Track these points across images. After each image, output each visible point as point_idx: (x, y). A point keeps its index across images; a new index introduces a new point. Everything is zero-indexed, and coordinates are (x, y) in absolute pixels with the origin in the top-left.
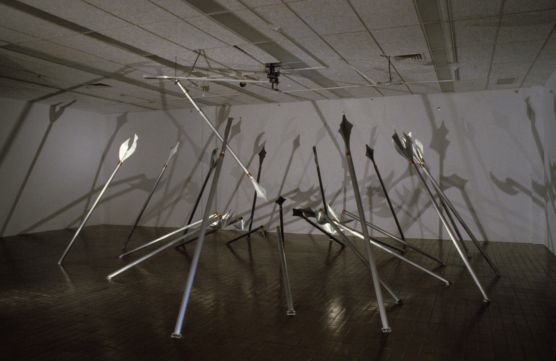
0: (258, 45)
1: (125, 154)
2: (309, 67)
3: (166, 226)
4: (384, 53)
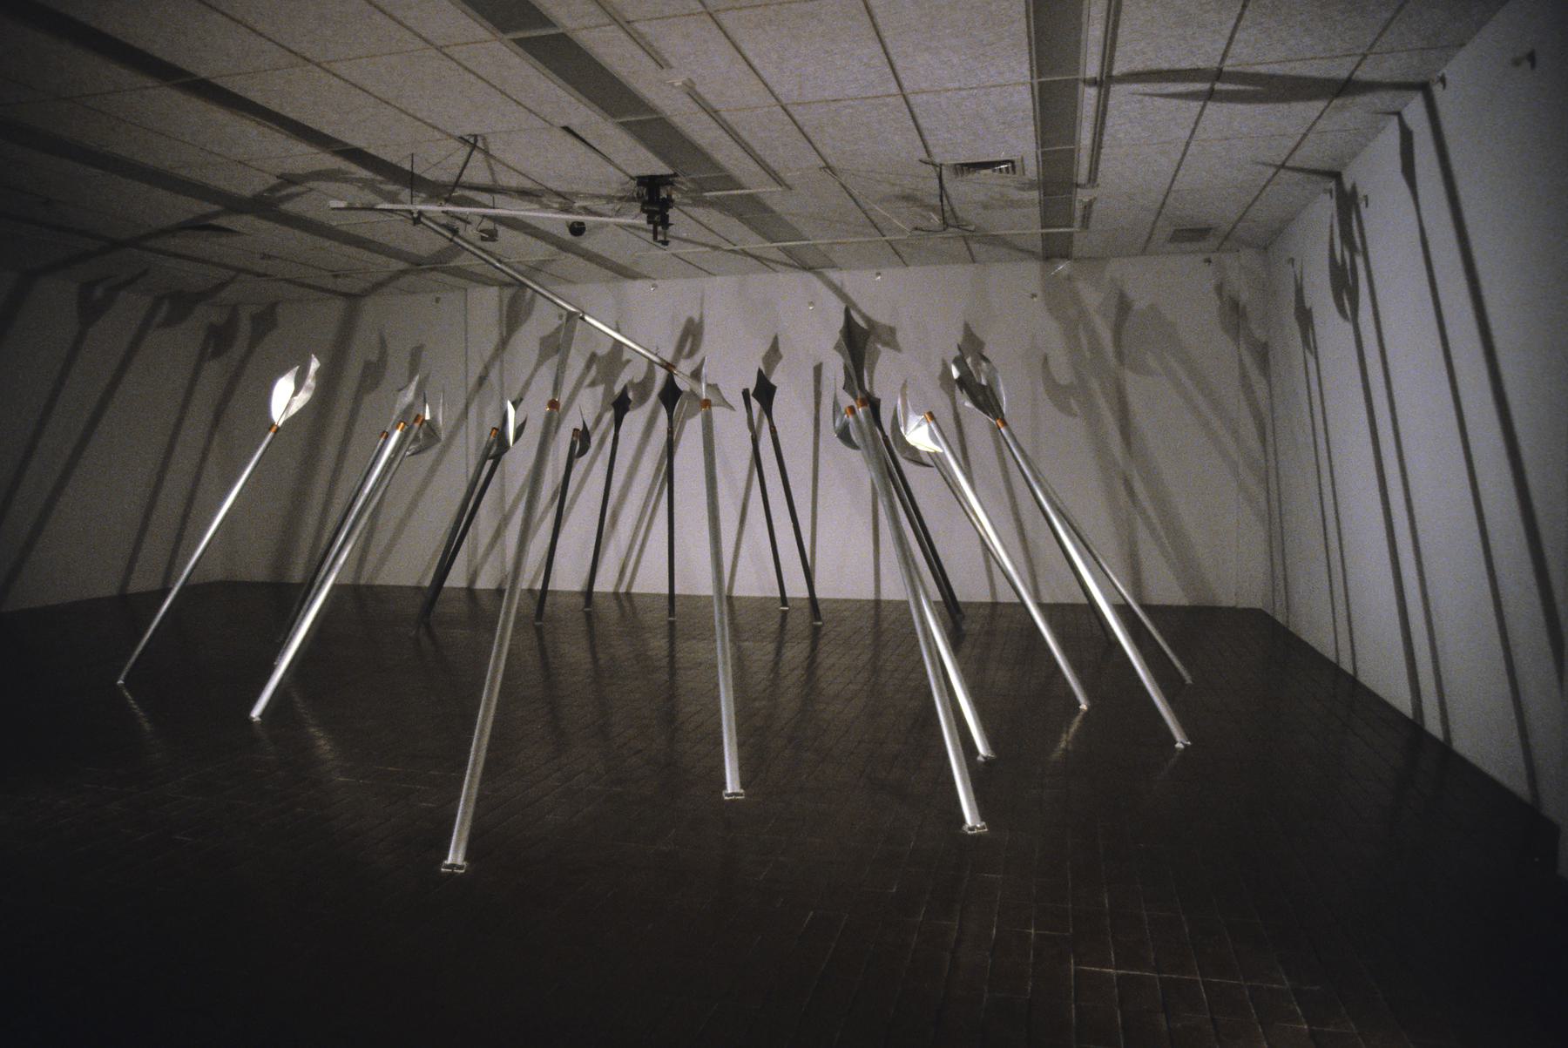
0: (626, 126)
1: (289, 406)
2: (743, 188)
3: (378, 582)
4: (929, 155)
